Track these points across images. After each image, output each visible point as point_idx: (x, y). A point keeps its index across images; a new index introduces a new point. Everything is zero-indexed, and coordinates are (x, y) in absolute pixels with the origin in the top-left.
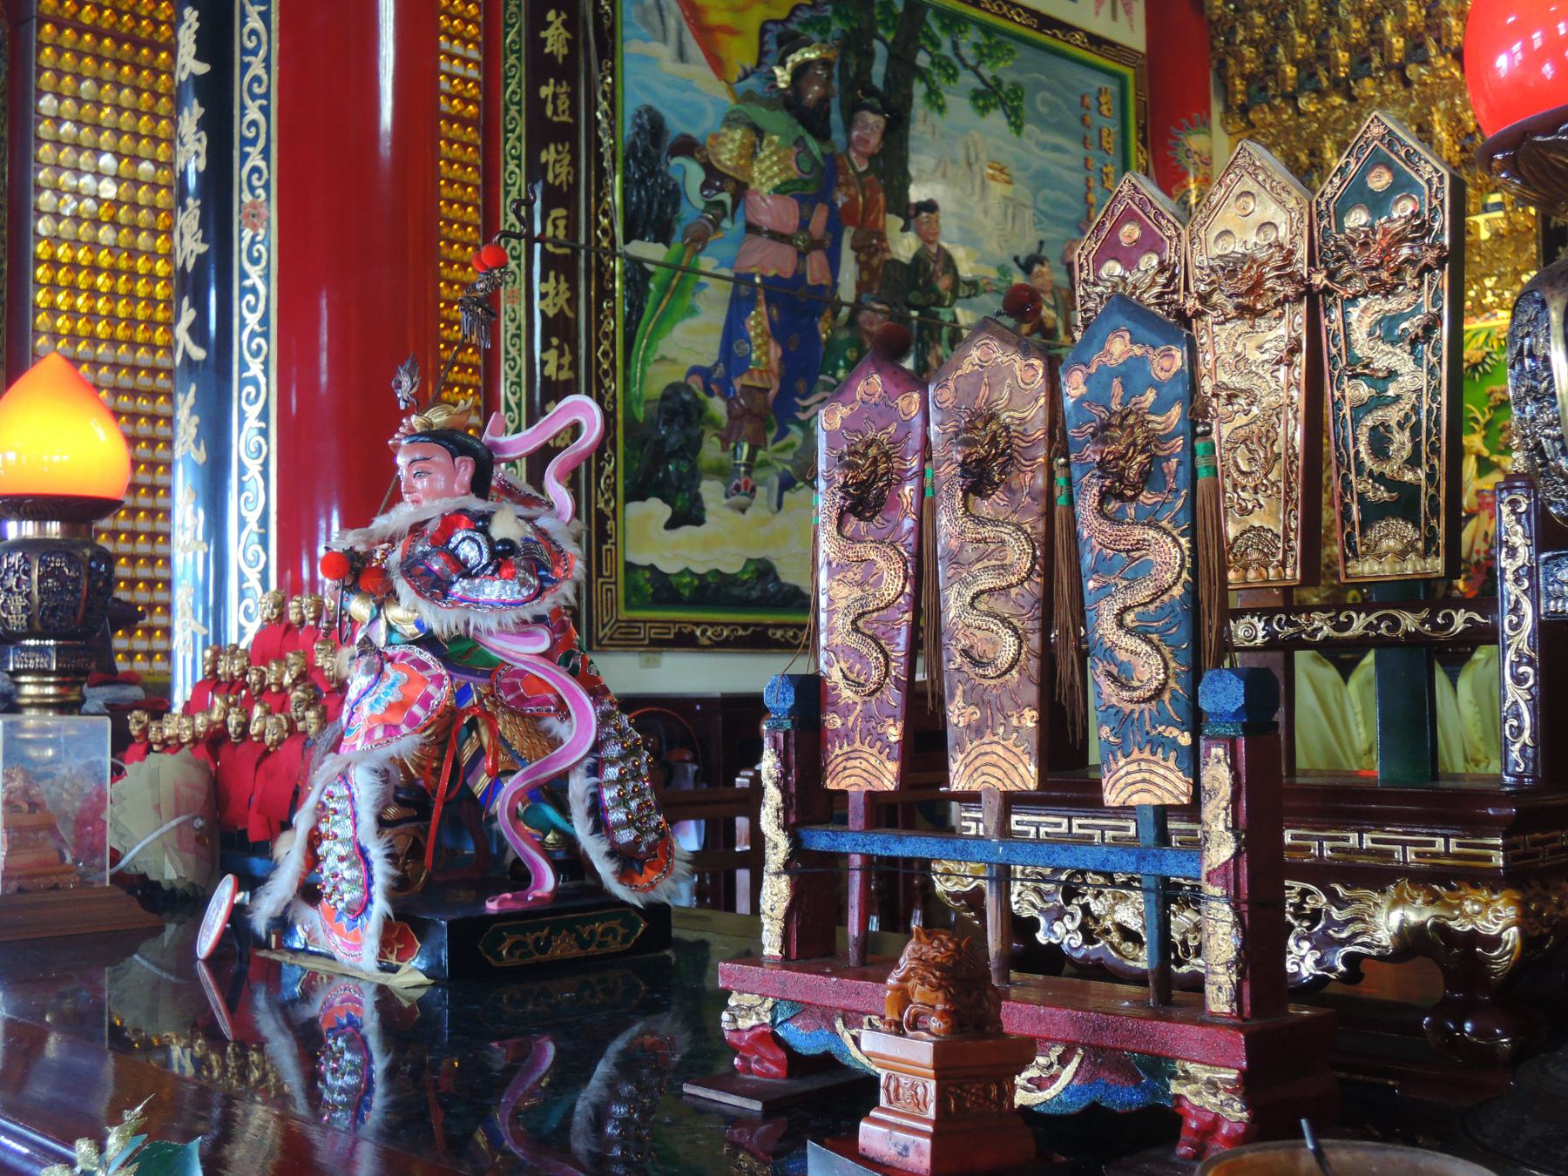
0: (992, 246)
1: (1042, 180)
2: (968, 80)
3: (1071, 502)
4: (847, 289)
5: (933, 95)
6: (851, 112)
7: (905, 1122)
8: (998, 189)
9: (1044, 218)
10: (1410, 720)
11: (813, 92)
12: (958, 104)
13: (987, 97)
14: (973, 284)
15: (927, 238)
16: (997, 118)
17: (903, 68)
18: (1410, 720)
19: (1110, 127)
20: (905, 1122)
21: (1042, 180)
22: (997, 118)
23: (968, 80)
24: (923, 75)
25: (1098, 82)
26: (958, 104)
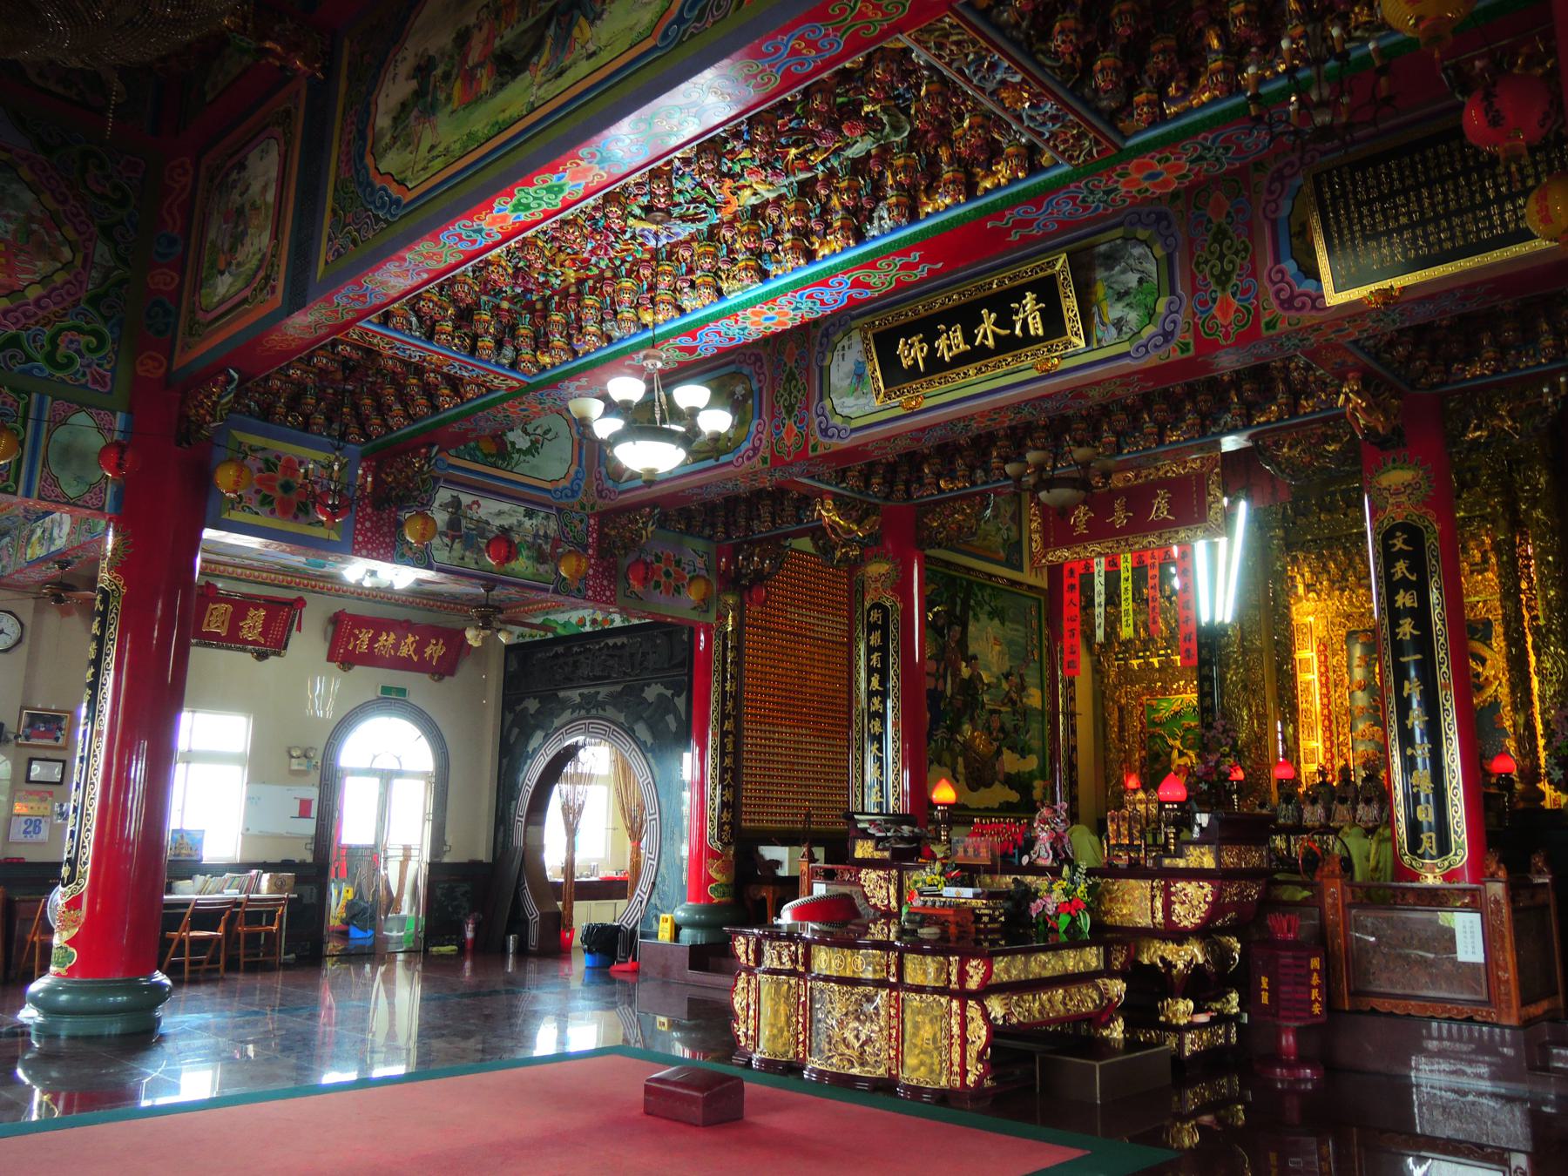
0: (995, 669)
1: (1011, 643)
2: (987, 608)
3: (256, 272)
4: (949, 692)
5: (975, 615)
6: (950, 625)
7: (109, 818)
8: (997, 648)
9: (1012, 658)
10: (1155, 839)
11: (940, 623)
12: (983, 617)
13: (992, 614)
14: (989, 685)
15: (974, 669)
16: (996, 622)
17: (966, 606)
18: (1155, 839)
19: (1035, 622)
20: (109, 818)
21: (1011, 643)
22: (996, 622)
23: (987, 608)
24: (973, 609)
25: (1030, 602)
26: (983, 617)
